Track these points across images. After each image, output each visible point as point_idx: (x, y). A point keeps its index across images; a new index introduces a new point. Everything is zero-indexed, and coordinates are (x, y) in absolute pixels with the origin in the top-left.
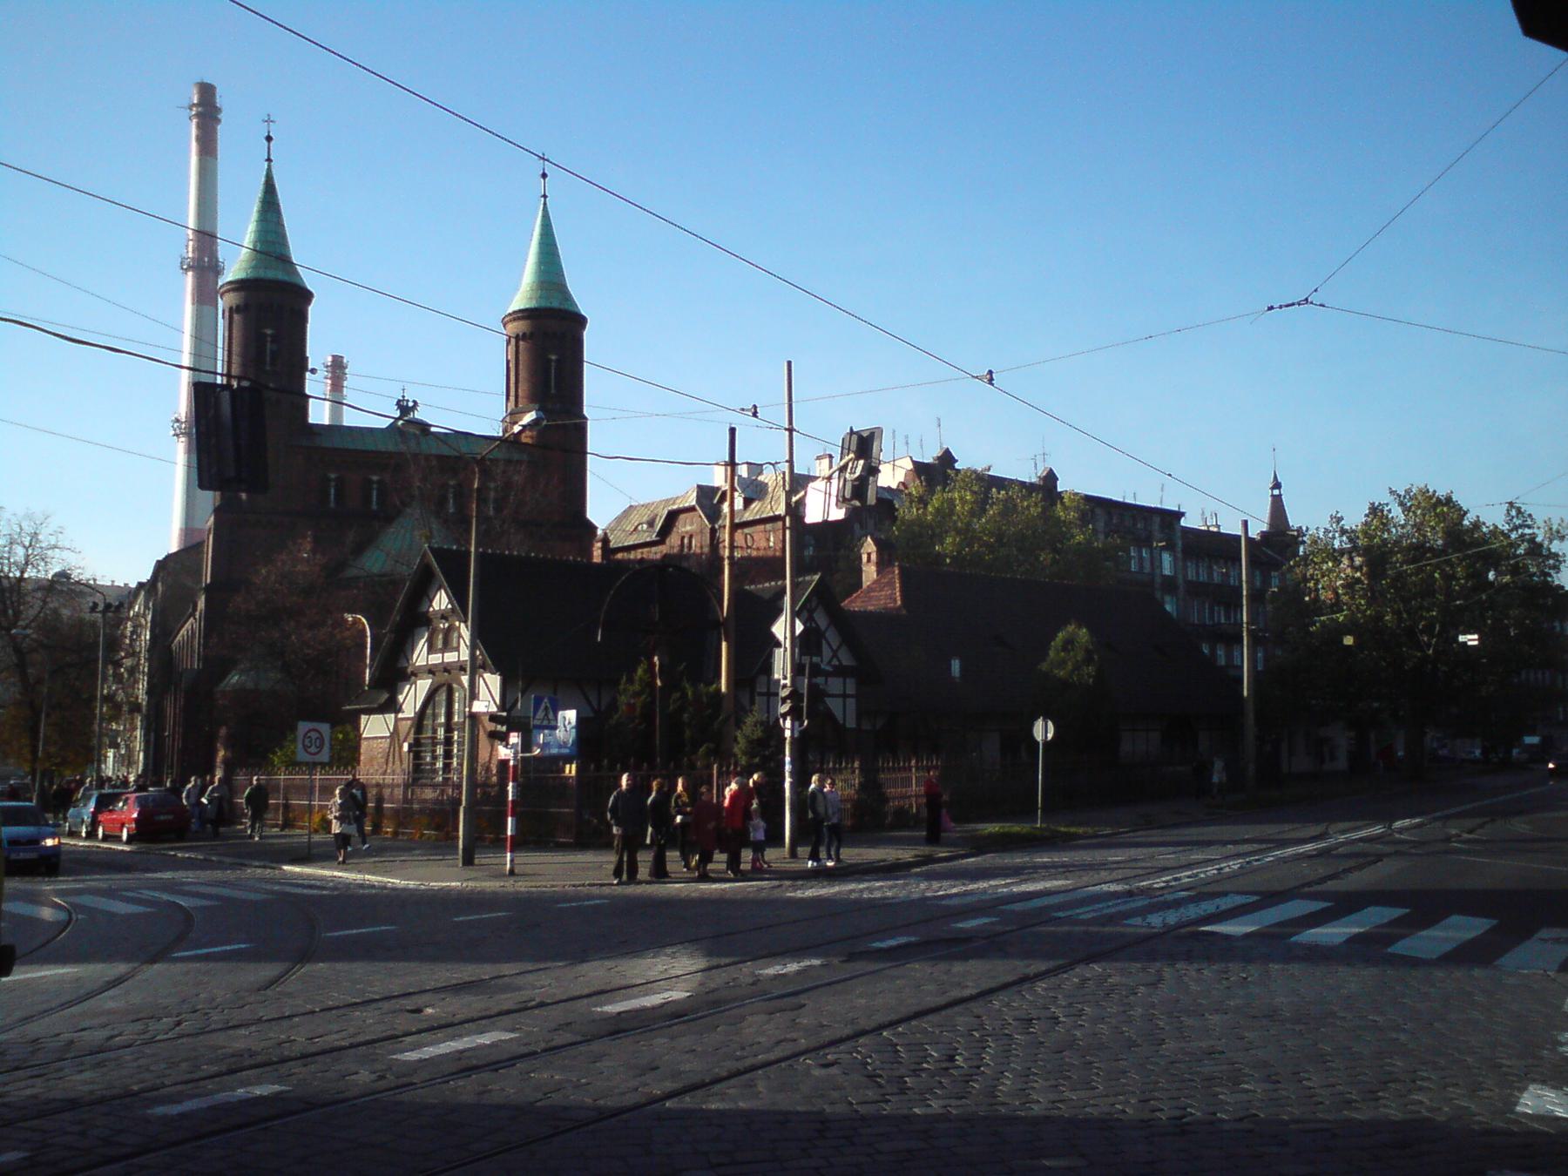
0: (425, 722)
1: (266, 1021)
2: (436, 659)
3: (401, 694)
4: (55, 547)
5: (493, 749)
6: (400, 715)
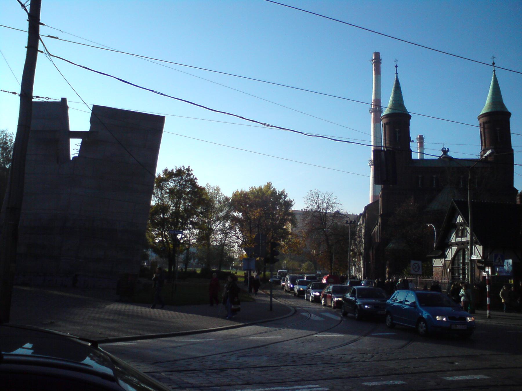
0: (455, 262)
1: (400, 359)
2: (459, 240)
3: (447, 252)
4: (335, 203)
5: (480, 273)
6: (446, 259)
